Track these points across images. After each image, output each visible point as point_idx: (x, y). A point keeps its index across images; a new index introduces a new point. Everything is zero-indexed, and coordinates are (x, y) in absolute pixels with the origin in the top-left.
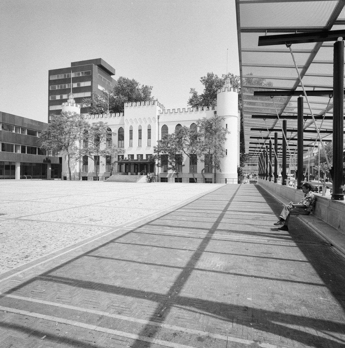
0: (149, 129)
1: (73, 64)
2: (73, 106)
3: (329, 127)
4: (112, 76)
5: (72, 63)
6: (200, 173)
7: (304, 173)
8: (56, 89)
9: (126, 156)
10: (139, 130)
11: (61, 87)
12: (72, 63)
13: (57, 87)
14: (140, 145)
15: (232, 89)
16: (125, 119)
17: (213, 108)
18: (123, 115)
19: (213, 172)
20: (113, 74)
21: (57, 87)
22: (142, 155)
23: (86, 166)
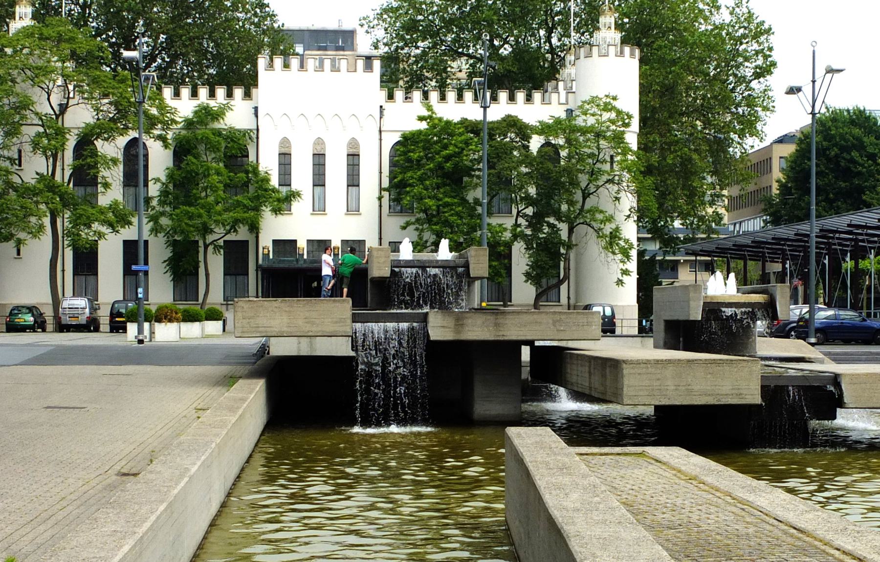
14: (319, 207)
17: (247, 95)
19: (564, 299)
23: (240, 278)
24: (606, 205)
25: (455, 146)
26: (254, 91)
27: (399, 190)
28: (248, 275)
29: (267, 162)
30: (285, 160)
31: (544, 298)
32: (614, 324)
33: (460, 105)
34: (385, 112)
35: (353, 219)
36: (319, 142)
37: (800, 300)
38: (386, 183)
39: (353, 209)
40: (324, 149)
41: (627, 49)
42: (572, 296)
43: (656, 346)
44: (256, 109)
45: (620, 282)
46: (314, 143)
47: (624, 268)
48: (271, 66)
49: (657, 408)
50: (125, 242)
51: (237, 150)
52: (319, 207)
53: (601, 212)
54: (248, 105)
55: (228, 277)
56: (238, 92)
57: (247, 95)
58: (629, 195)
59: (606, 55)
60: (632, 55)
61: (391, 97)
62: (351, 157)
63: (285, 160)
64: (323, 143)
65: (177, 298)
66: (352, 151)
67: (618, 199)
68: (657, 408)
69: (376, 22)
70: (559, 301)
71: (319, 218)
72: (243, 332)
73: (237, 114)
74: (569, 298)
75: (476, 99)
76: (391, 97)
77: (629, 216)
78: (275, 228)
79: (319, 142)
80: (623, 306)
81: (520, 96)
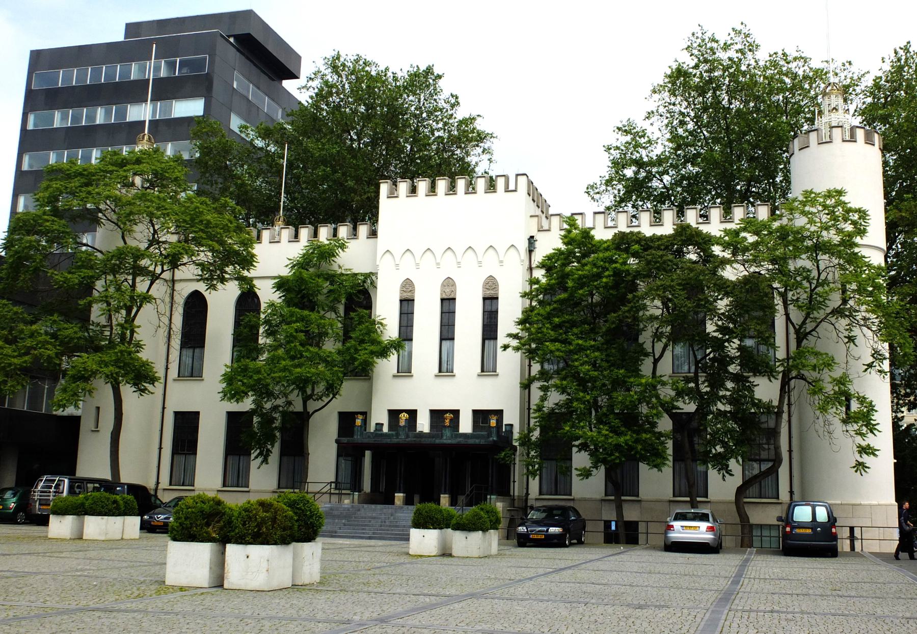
0: (487, 296)
1: (132, 29)
2: (853, 139)
3: (173, 343)
4: (287, 84)
5: (128, 26)
6: (730, 502)
7: (453, 503)
8: (98, 122)
9: (379, 417)
10: (442, 300)
11: (76, 118)
12: (128, 26)
13: (58, 120)
14: (445, 368)
15: (860, 134)
16: (380, 252)
18: (373, 234)
20: (294, 76)
21: (58, 120)
22: (413, 414)
24: (838, 351)
25: (595, 265)
27: (537, 335)
29: (386, 309)
30: (407, 305)
31: (754, 490)
32: (835, 537)
34: (537, 244)
35: (488, 382)
36: (449, 283)
37: (226, 517)
39: (488, 367)
40: (454, 291)
42: (795, 489)
45: (860, 467)
46: (443, 285)
47: (864, 444)
48: (392, 195)
51: (359, 294)
52: (445, 368)
53: (817, 354)
55: (285, 459)
58: (869, 333)
62: (488, 302)
63: (407, 305)
64: (454, 284)
65: (283, 483)
66: (490, 293)
67: (851, 339)
69: (604, 187)
70: (778, 498)
71: (445, 382)
72: (374, 533)
73: (355, 255)
74: (791, 492)
77: (870, 366)
79: (449, 283)
80: (871, 506)
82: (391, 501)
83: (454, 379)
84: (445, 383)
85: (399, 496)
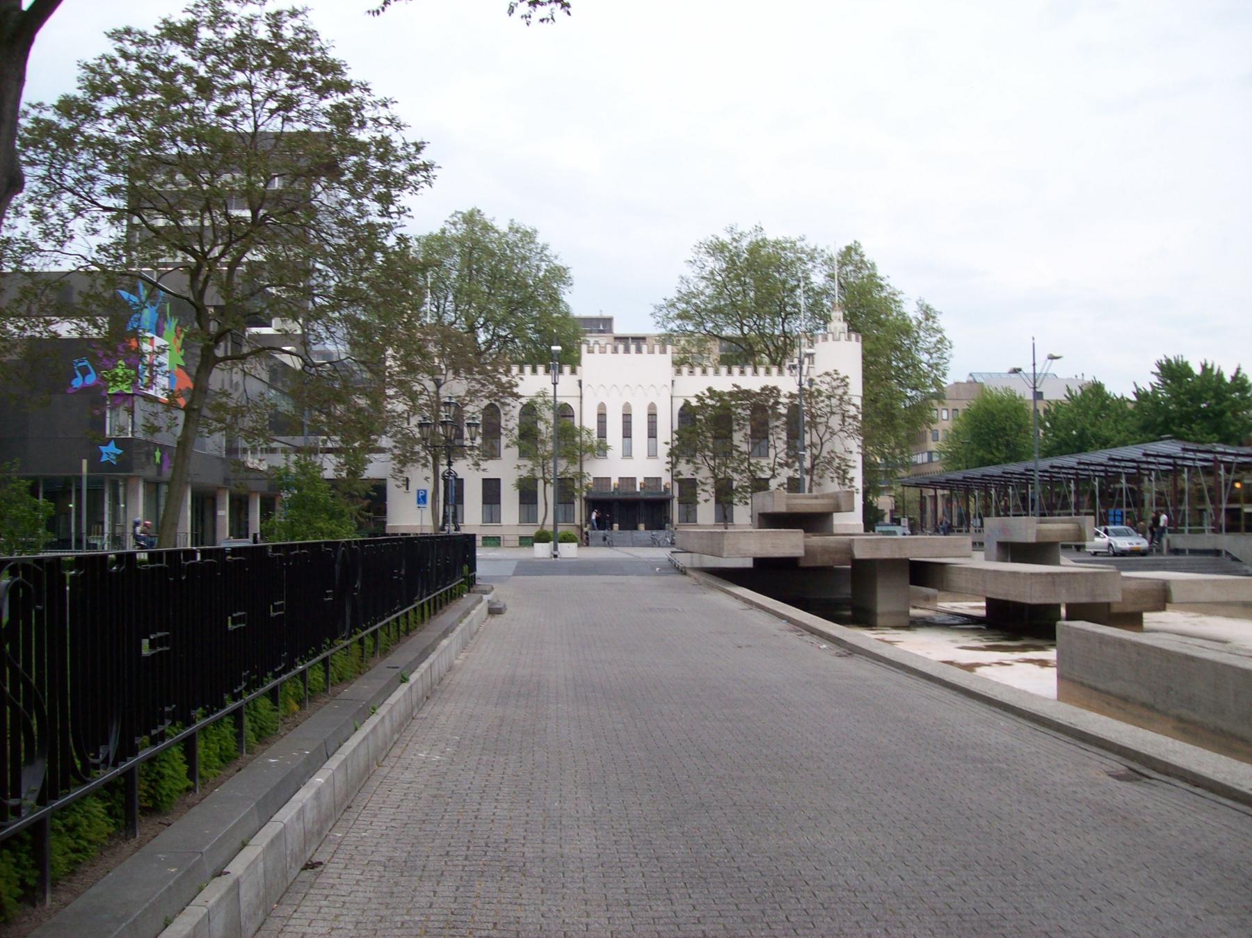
14: (628, 454)
17: (573, 372)
26: (578, 368)
28: (536, 503)
30: (602, 418)
33: (768, 378)
38: (676, 427)
39: (652, 454)
41: (853, 336)
43: (987, 559)
44: (580, 382)
49: (756, 560)
50: (498, 480)
52: (628, 454)
54: (575, 378)
56: (567, 369)
57: (573, 372)
59: (839, 340)
60: (857, 340)
61: (679, 372)
63: (602, 418)
68: (756, 560)
73: (566, 387)
75: (547, 372)
76: (679, 372)
78: (596, 469)
81: (749, 370)
82: (636, 528)
83: (635, 463)
84: (627, 462)
85: (616, 526)
